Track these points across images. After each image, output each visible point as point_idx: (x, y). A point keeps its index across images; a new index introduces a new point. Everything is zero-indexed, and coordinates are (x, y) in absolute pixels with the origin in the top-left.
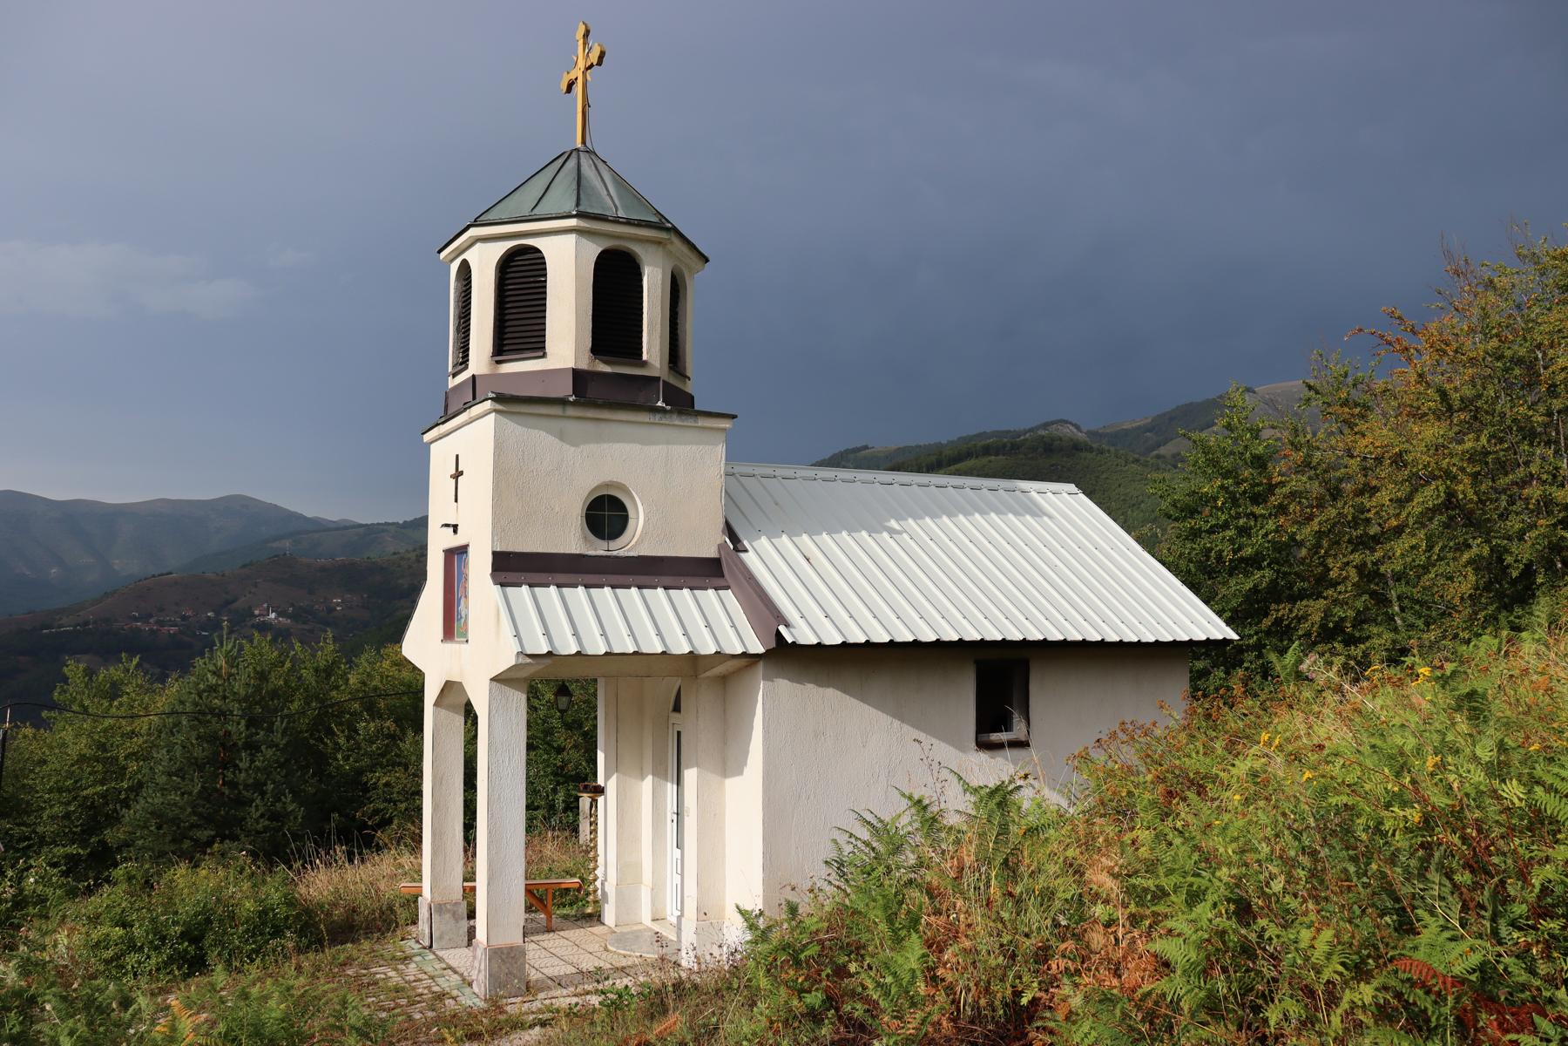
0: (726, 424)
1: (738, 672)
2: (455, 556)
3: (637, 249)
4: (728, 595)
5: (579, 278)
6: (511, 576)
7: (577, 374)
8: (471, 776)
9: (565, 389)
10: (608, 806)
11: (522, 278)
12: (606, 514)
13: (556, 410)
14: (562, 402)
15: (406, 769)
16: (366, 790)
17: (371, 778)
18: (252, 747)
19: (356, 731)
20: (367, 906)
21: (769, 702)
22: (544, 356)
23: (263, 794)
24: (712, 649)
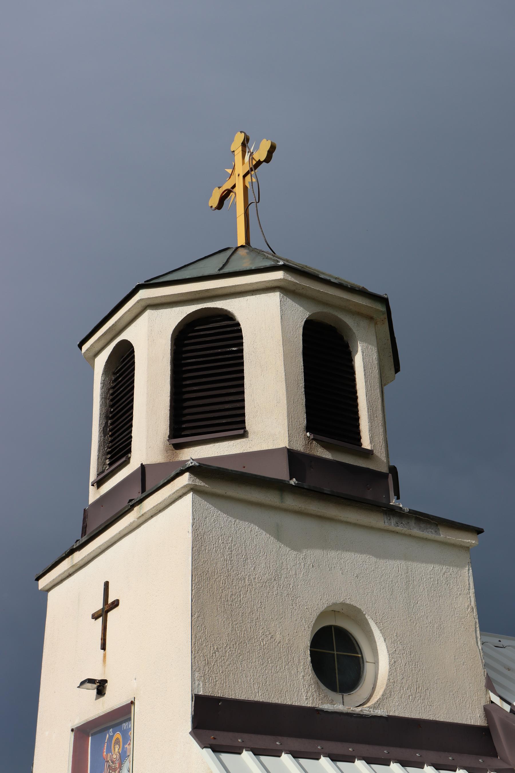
0: (470, 540)
3: (349, 321)
7: (293, 456)
9: (281, 471)
13: (270, 498)
22: (244, 435)
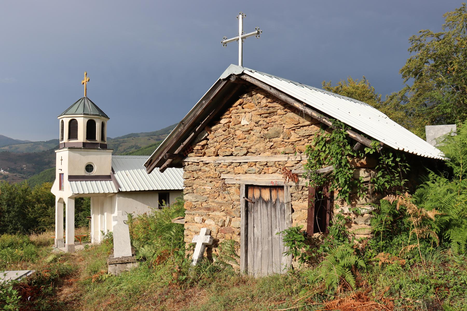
1: (113, 196)
2: (61, 175)
4: (112, 182)
5: (84, 125)
6: (71, 180)
7: (83, 143)
8: (64, 214)
9: (81, 146)
10: (92, 219)
11: (73, 125)
12: (89, 168)
13: (80, 150)
14: (81, 148)
15: (49, 216)
16: (38, 222)
17: (39, 219)
18: (9, 212)
19: (35, 207)
20: (44, 241)
21: (118, 200)
23: (12, 223)
24: (107, 192)
